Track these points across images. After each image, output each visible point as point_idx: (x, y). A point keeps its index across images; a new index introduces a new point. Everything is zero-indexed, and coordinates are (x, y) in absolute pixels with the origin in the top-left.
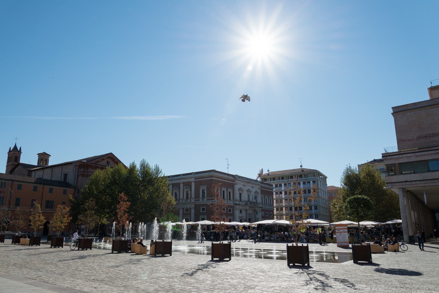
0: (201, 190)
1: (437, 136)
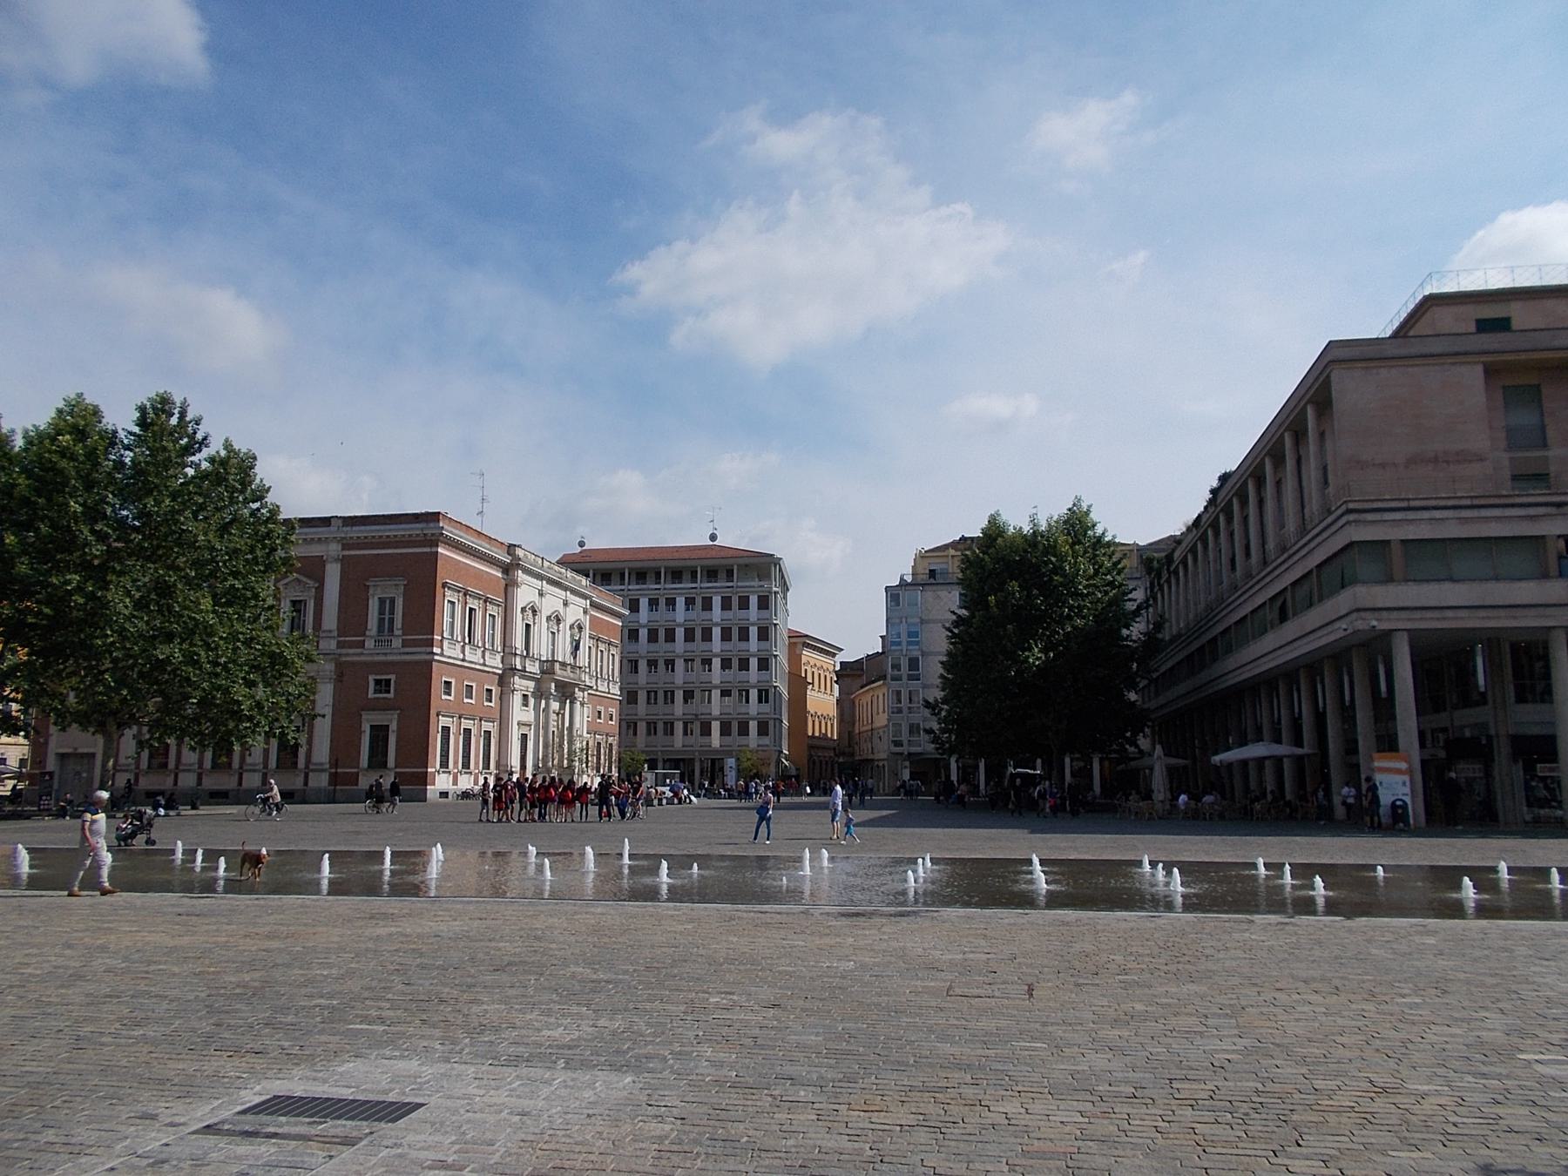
1: (1470, 461)
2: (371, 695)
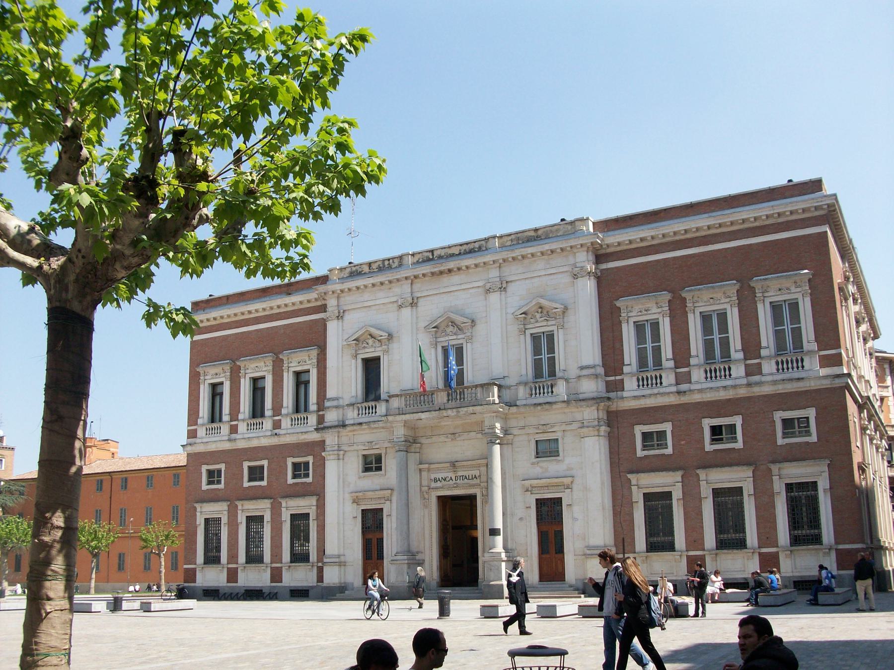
0: (248, 376)
2: (640, 453)
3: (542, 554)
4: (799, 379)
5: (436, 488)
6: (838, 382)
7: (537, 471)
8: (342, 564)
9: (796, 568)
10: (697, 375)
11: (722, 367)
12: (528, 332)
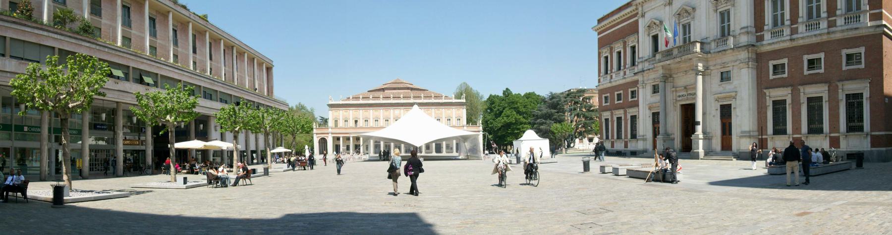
3: (723, 135)
4: (856, 29)
5: (679, 101)
6: (879, 30)
7: (721, 89)
8: (644, 140)
9: (848, 146)
10: (802, 28)
11: (815, 23)
12: (718, 11)
